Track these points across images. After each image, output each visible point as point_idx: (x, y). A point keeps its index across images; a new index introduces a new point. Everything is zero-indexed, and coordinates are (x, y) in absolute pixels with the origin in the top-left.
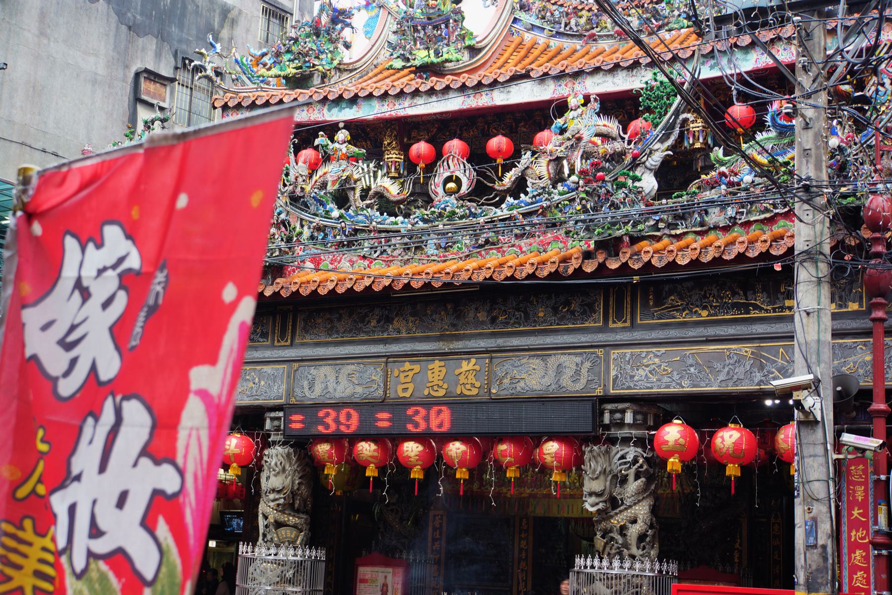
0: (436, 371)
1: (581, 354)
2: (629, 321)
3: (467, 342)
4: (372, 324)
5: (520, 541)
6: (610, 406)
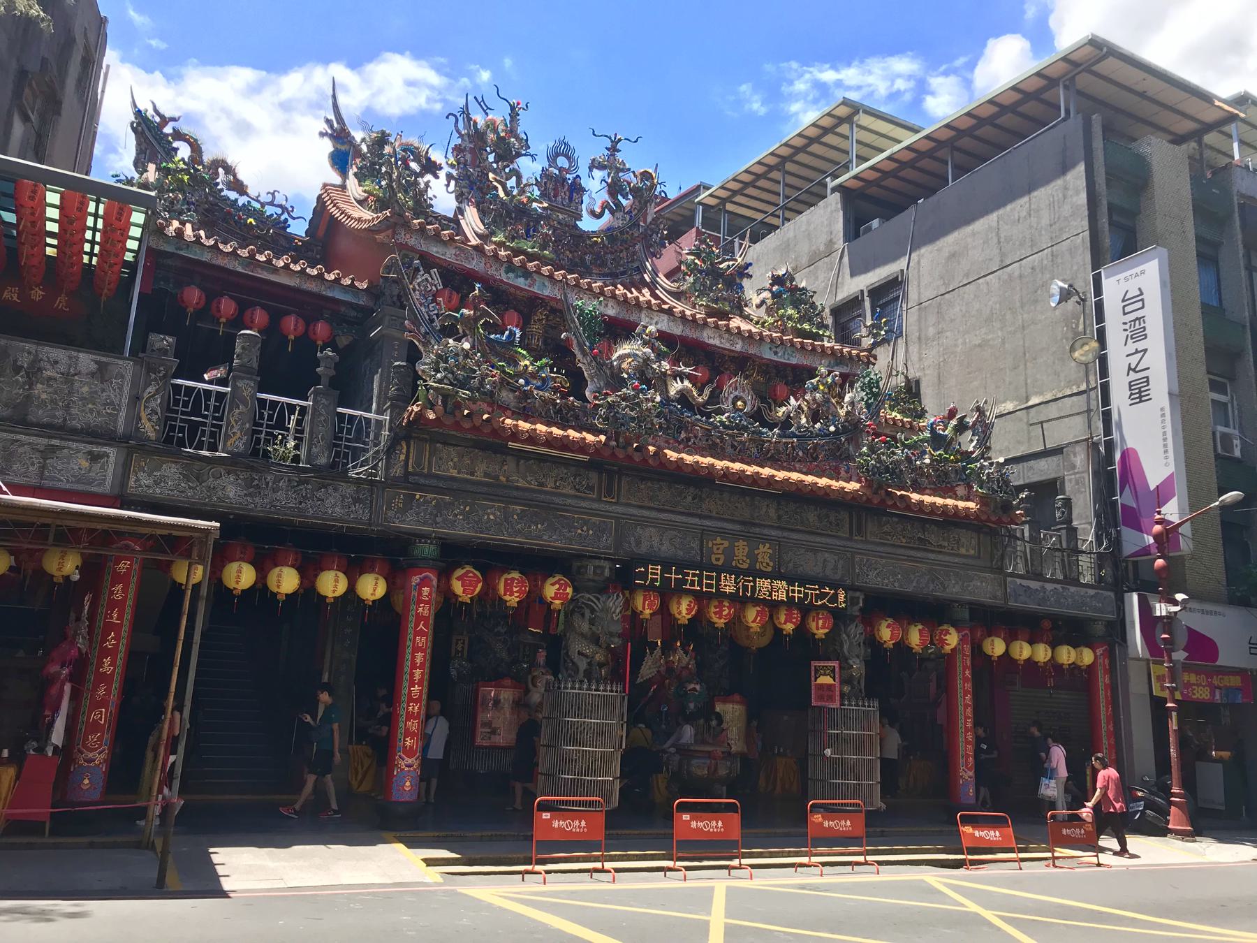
0: (741, 548)
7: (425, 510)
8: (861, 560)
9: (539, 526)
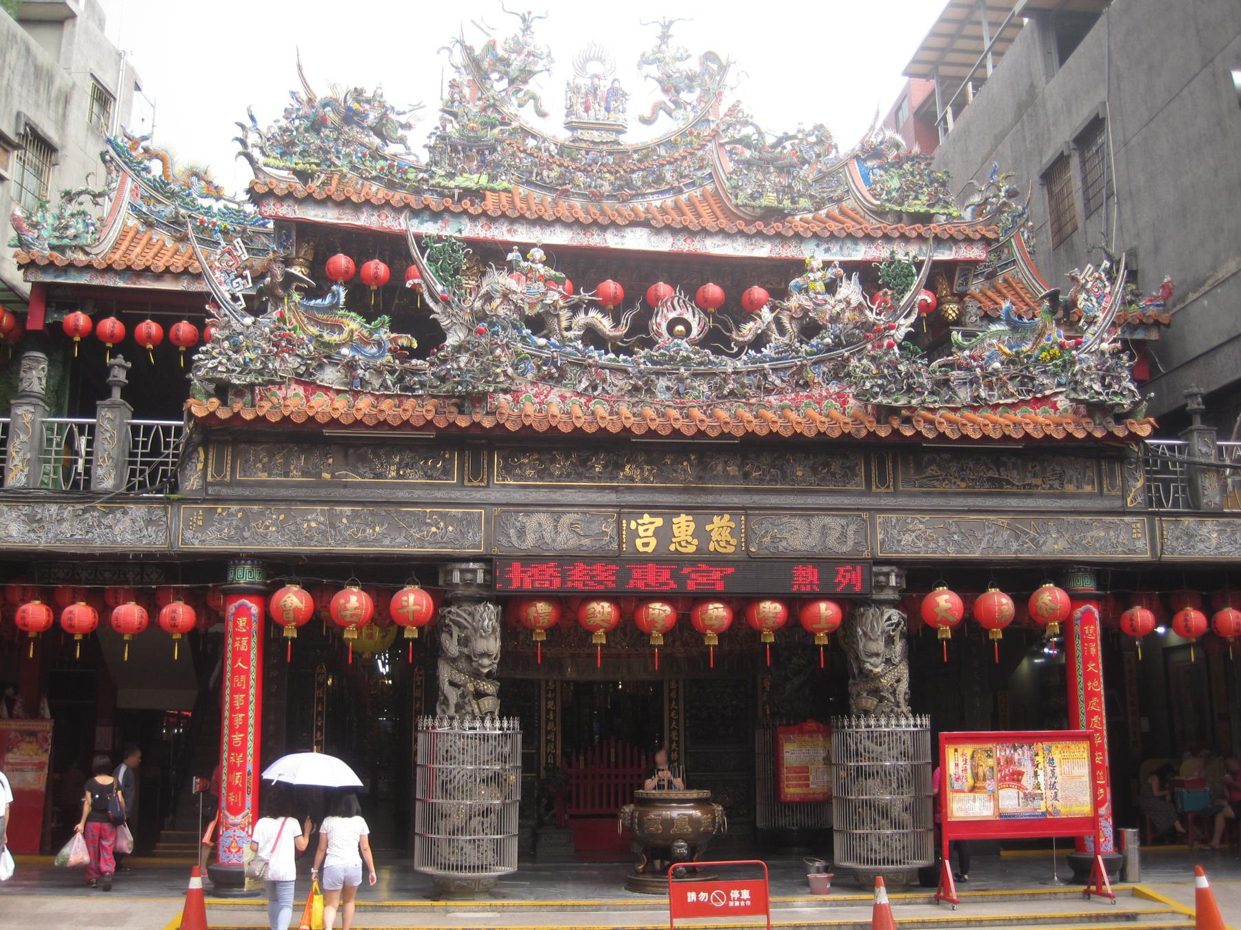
1: (846, 516)
2: (892, 487)
3: (718, 497)
4: (597, 469)
5: (547, 701)
6: (458, 566)
7: (229, 526)
8: (885, 521)
9: (377, 529)
